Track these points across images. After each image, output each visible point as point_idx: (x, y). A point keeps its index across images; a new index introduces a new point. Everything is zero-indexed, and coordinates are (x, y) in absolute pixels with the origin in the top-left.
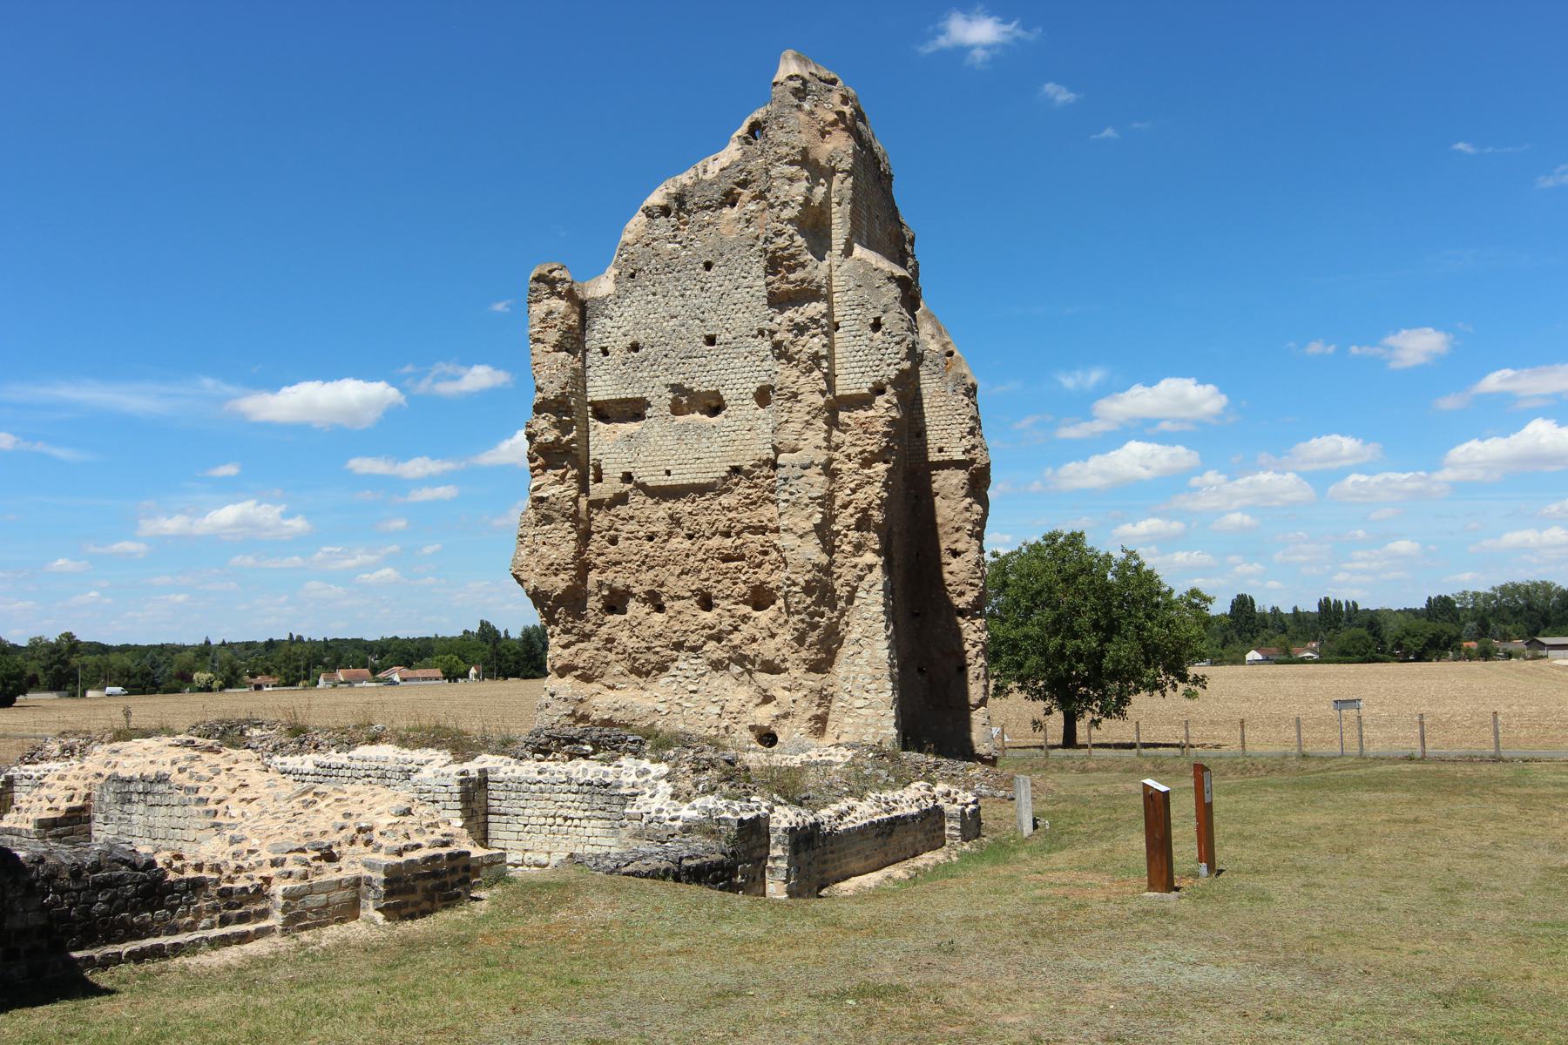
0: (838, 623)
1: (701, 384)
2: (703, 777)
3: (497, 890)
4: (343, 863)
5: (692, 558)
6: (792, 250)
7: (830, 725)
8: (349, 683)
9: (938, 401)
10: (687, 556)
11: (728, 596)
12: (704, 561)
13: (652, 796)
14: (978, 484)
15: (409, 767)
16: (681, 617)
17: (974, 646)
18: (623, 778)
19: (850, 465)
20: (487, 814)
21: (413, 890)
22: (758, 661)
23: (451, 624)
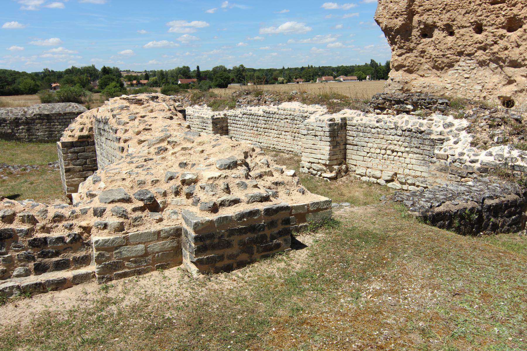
2: (497, 131)
3: (320, 235)
4: (165, 214)
5: (473, 4)
8: (326, 81)
11: (493, 24)
12: (480, 5)
13: (456, 143)
15: (305, 115)
16: (463, 38)
18: (434, 128)
20: (346, 144)
21: (229, 245)
22: (508, 60)
23: (362, 61)
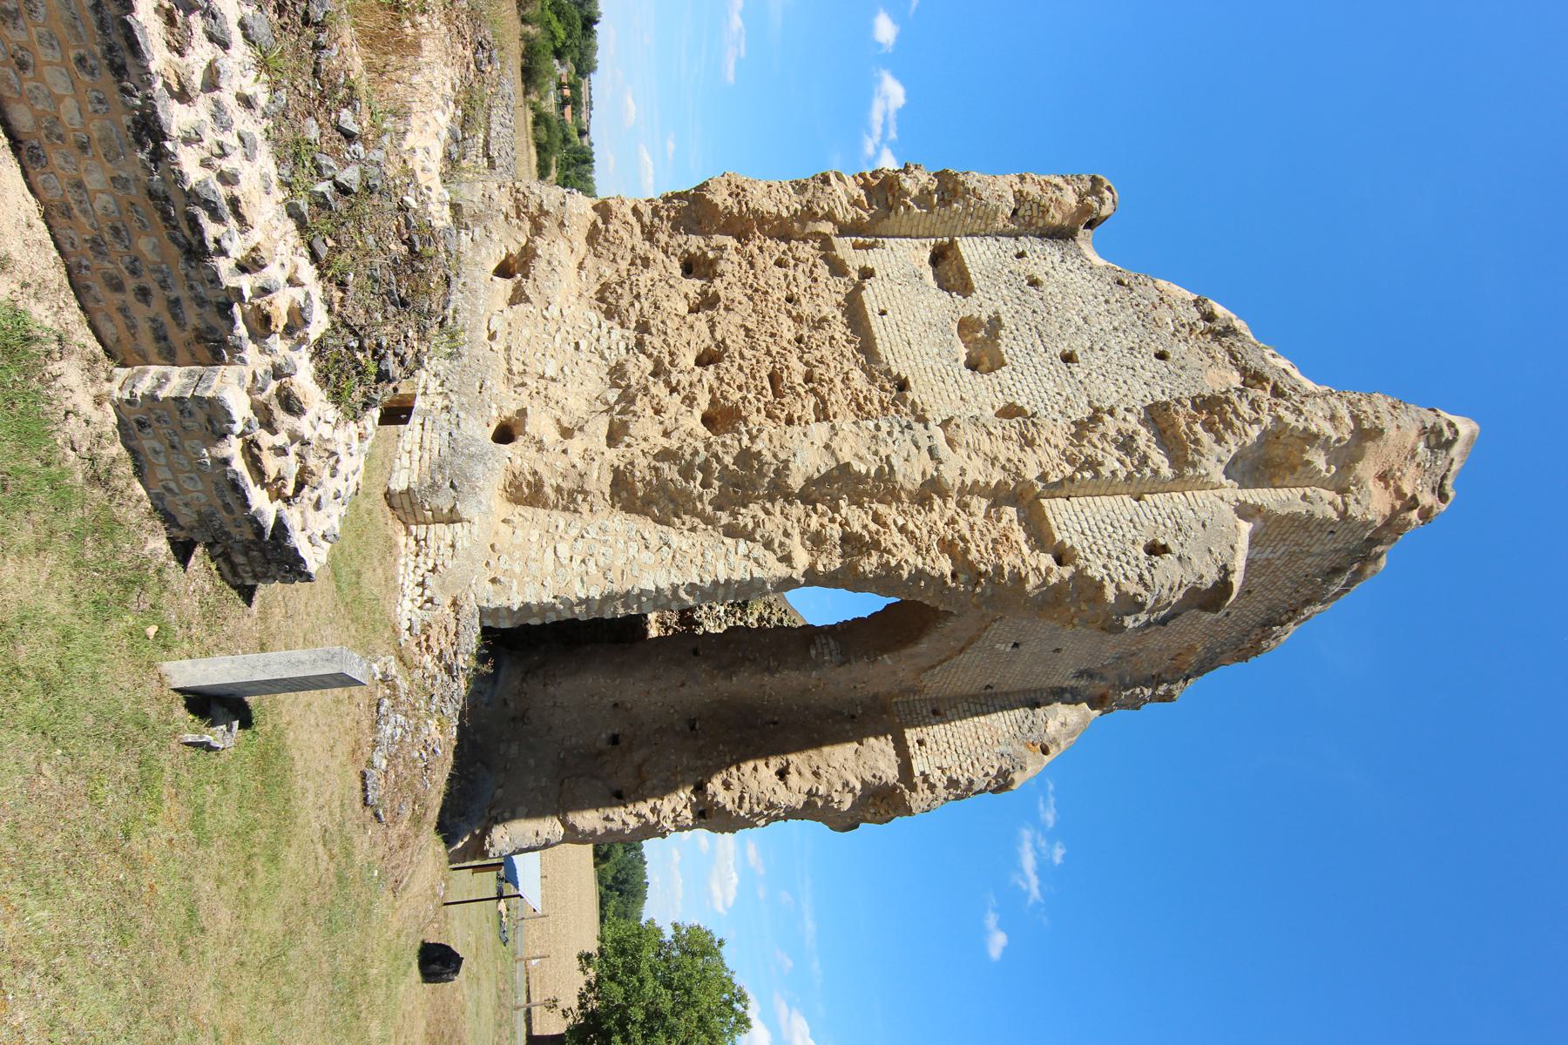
0: (694, 513)
6: (1238, 423)
7: (528, 511)
9: (985, 734)
10: (773, 335)
11: (722, 380)
12: (768, 353)
14: (881, 802)
16: (685, 328)
17: (653, 810)
19: (940, 525)
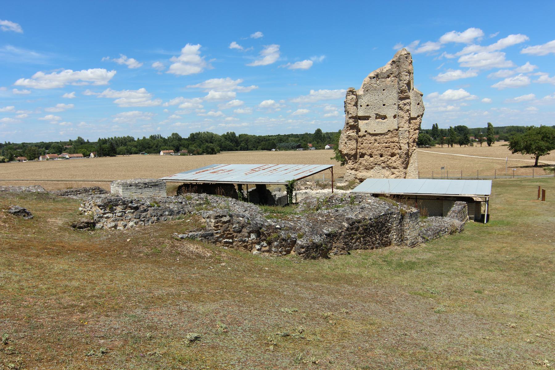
1: (382, 114)
